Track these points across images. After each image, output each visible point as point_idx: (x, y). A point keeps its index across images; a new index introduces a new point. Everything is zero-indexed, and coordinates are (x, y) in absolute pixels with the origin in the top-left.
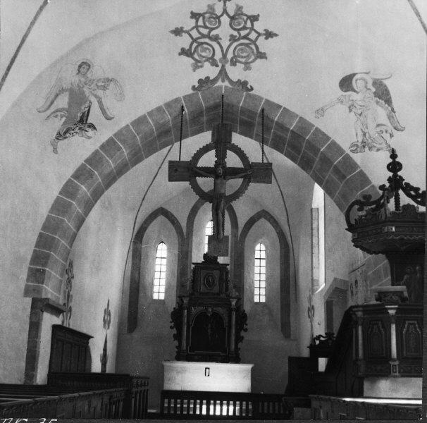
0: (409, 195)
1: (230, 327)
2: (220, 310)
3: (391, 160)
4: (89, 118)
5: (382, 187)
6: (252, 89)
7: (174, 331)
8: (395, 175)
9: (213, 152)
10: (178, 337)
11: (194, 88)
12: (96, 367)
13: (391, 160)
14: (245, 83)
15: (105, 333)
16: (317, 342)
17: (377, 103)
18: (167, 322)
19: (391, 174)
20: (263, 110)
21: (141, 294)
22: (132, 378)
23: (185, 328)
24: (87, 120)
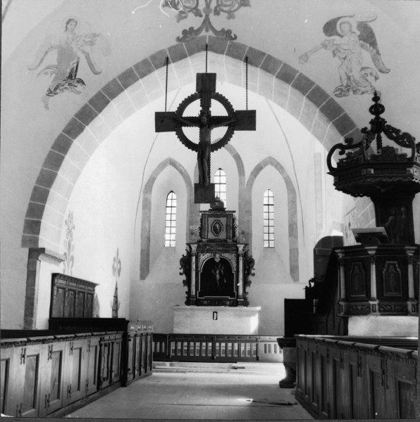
7: (184, 277)
17: (362, 46)
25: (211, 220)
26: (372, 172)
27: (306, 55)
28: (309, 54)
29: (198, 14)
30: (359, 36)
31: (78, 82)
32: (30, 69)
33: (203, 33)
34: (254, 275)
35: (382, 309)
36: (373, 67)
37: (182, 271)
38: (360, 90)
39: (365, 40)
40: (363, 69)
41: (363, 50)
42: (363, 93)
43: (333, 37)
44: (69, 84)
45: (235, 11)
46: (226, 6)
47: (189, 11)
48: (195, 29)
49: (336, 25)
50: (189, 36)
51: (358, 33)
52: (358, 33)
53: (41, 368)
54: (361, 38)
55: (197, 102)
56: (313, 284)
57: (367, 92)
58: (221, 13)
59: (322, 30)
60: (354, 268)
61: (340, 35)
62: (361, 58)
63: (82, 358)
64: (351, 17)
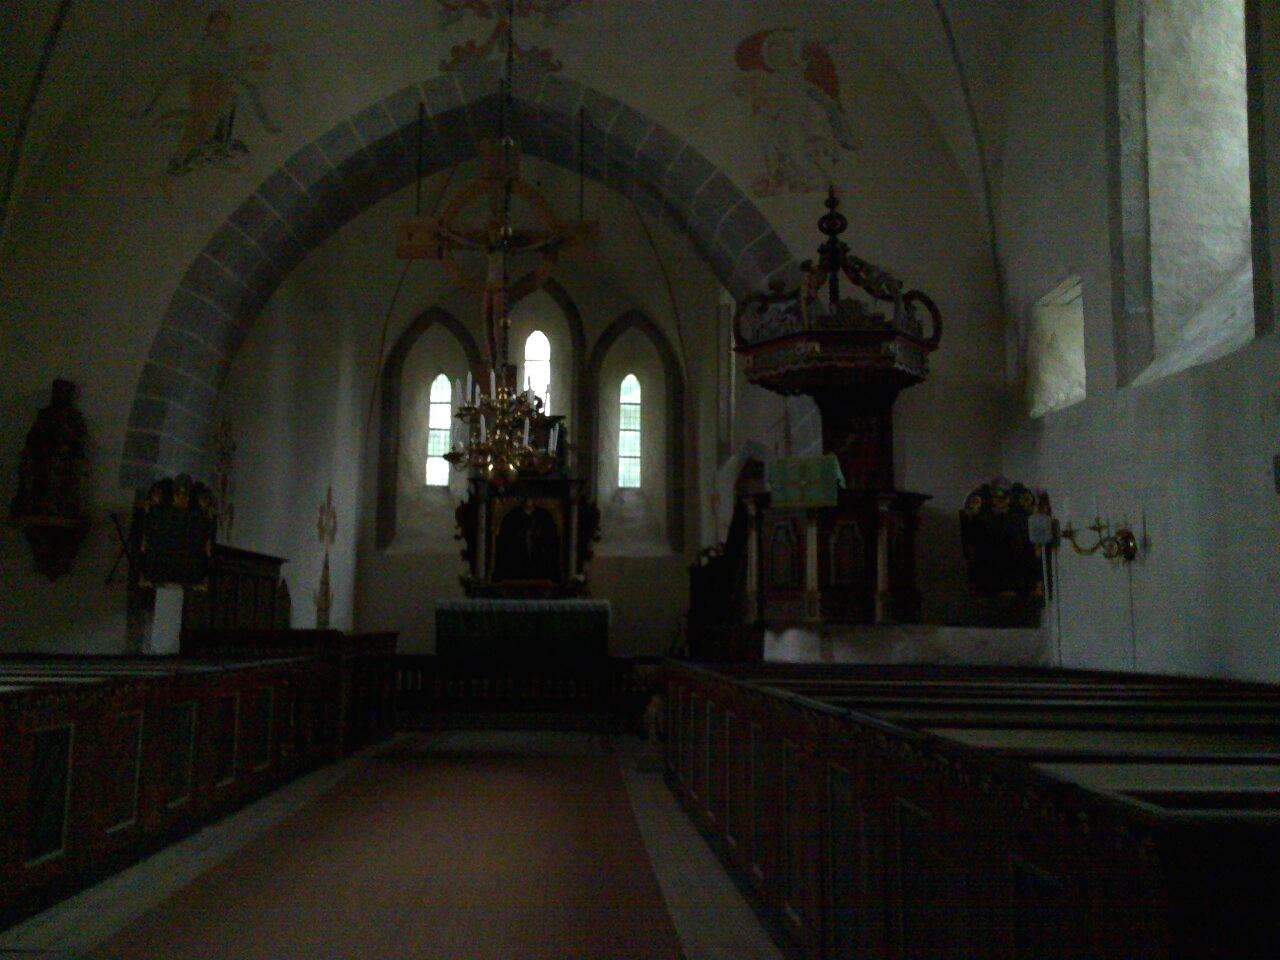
0: (856, 281)
1: (567, 535)
2: (551, 504)
3: (826, 211)
4: (234, 132)
5: (806, 266)
6: (559, 67)
7: (463, 545)
8: (833, 241)
9: (1081, 299)
10: (469, 555)
11: (445, 66)
12: (304, 617)
13: (826, 211)
14: (546, 55)
15: (321, 555)
16: (704, 561)
17: (809, 93)
18: (448, 525)
19: (824, 238)
20: (582, 111)
21: (402, 477)
22: (1043, 417)
23: (483, 536)
24: (229, 134)
37: (459, 532)
42: (808, 190)
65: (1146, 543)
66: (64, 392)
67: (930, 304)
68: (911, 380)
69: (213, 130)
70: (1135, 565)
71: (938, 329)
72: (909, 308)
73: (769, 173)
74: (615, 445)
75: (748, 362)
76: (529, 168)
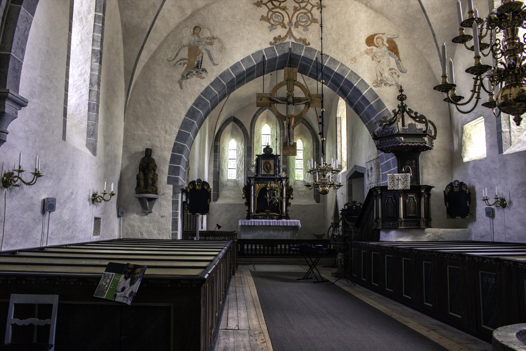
6: (309, 44)
7: (245, 201)
17: (390, 54)
19: (399, 102)
25: (263, 162)
26: (403, 139)
27: (355, 58)
28: (357, 58)
29: (284, 26)
30: (388, 48)
31: (203, 71)
32: (169, 61)
33: (287, 40)
34: (292, 199)
35: (405, 225)
36: (396, 68)
37: (244, 196)
38: (388, 83)
39: (392, 51)
40: (390, 69)
41: (391, 57)
42: (390, 85)
43: (371, 47)
44: (196, 72)
45: (308, 25)
46: (303, 22)
47: (278, 24)
48: (282, 37)
49: (373, 39)
50: (278, 41)
51: (388, 45)
52: (388, 45)
53: (66, 242)
54: (389, 48)
55: (285, 87)
56: (346, 207)
57: (392, 85)
58: (299, 26)
59: (365, 42)
60: (388, 200)
61: (376, 46)
62: (390, 62)
63: (50, 220)
64: (383, 34)
65: (510, 202)
66: (148, 152)
67: (433, 124)
68: (428, 148)
69: (196, 65)
70: (506, 210)
71: (436, 132)
72: (427, 126)
73: (378, 80)
74: (294, 165)
75: (378, 143)
76: (300, 78)
